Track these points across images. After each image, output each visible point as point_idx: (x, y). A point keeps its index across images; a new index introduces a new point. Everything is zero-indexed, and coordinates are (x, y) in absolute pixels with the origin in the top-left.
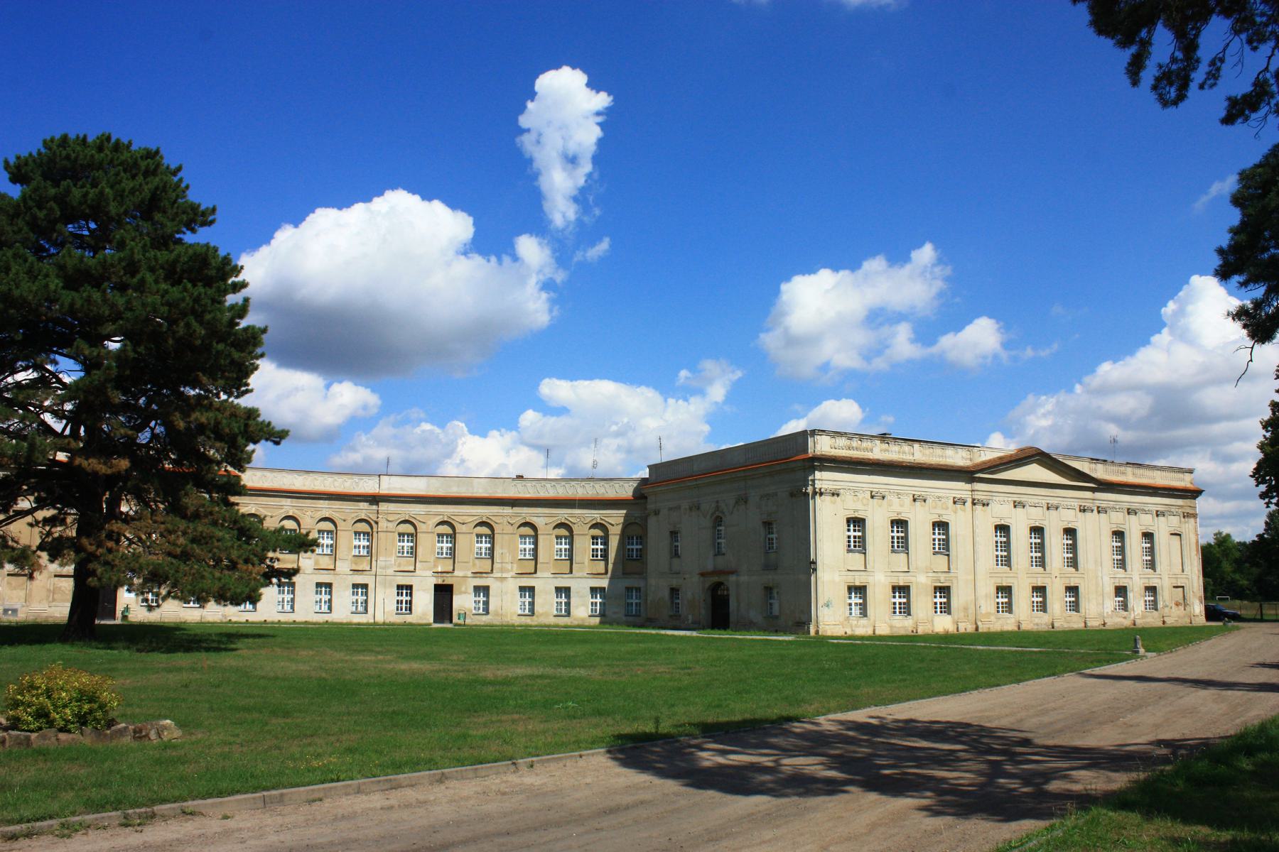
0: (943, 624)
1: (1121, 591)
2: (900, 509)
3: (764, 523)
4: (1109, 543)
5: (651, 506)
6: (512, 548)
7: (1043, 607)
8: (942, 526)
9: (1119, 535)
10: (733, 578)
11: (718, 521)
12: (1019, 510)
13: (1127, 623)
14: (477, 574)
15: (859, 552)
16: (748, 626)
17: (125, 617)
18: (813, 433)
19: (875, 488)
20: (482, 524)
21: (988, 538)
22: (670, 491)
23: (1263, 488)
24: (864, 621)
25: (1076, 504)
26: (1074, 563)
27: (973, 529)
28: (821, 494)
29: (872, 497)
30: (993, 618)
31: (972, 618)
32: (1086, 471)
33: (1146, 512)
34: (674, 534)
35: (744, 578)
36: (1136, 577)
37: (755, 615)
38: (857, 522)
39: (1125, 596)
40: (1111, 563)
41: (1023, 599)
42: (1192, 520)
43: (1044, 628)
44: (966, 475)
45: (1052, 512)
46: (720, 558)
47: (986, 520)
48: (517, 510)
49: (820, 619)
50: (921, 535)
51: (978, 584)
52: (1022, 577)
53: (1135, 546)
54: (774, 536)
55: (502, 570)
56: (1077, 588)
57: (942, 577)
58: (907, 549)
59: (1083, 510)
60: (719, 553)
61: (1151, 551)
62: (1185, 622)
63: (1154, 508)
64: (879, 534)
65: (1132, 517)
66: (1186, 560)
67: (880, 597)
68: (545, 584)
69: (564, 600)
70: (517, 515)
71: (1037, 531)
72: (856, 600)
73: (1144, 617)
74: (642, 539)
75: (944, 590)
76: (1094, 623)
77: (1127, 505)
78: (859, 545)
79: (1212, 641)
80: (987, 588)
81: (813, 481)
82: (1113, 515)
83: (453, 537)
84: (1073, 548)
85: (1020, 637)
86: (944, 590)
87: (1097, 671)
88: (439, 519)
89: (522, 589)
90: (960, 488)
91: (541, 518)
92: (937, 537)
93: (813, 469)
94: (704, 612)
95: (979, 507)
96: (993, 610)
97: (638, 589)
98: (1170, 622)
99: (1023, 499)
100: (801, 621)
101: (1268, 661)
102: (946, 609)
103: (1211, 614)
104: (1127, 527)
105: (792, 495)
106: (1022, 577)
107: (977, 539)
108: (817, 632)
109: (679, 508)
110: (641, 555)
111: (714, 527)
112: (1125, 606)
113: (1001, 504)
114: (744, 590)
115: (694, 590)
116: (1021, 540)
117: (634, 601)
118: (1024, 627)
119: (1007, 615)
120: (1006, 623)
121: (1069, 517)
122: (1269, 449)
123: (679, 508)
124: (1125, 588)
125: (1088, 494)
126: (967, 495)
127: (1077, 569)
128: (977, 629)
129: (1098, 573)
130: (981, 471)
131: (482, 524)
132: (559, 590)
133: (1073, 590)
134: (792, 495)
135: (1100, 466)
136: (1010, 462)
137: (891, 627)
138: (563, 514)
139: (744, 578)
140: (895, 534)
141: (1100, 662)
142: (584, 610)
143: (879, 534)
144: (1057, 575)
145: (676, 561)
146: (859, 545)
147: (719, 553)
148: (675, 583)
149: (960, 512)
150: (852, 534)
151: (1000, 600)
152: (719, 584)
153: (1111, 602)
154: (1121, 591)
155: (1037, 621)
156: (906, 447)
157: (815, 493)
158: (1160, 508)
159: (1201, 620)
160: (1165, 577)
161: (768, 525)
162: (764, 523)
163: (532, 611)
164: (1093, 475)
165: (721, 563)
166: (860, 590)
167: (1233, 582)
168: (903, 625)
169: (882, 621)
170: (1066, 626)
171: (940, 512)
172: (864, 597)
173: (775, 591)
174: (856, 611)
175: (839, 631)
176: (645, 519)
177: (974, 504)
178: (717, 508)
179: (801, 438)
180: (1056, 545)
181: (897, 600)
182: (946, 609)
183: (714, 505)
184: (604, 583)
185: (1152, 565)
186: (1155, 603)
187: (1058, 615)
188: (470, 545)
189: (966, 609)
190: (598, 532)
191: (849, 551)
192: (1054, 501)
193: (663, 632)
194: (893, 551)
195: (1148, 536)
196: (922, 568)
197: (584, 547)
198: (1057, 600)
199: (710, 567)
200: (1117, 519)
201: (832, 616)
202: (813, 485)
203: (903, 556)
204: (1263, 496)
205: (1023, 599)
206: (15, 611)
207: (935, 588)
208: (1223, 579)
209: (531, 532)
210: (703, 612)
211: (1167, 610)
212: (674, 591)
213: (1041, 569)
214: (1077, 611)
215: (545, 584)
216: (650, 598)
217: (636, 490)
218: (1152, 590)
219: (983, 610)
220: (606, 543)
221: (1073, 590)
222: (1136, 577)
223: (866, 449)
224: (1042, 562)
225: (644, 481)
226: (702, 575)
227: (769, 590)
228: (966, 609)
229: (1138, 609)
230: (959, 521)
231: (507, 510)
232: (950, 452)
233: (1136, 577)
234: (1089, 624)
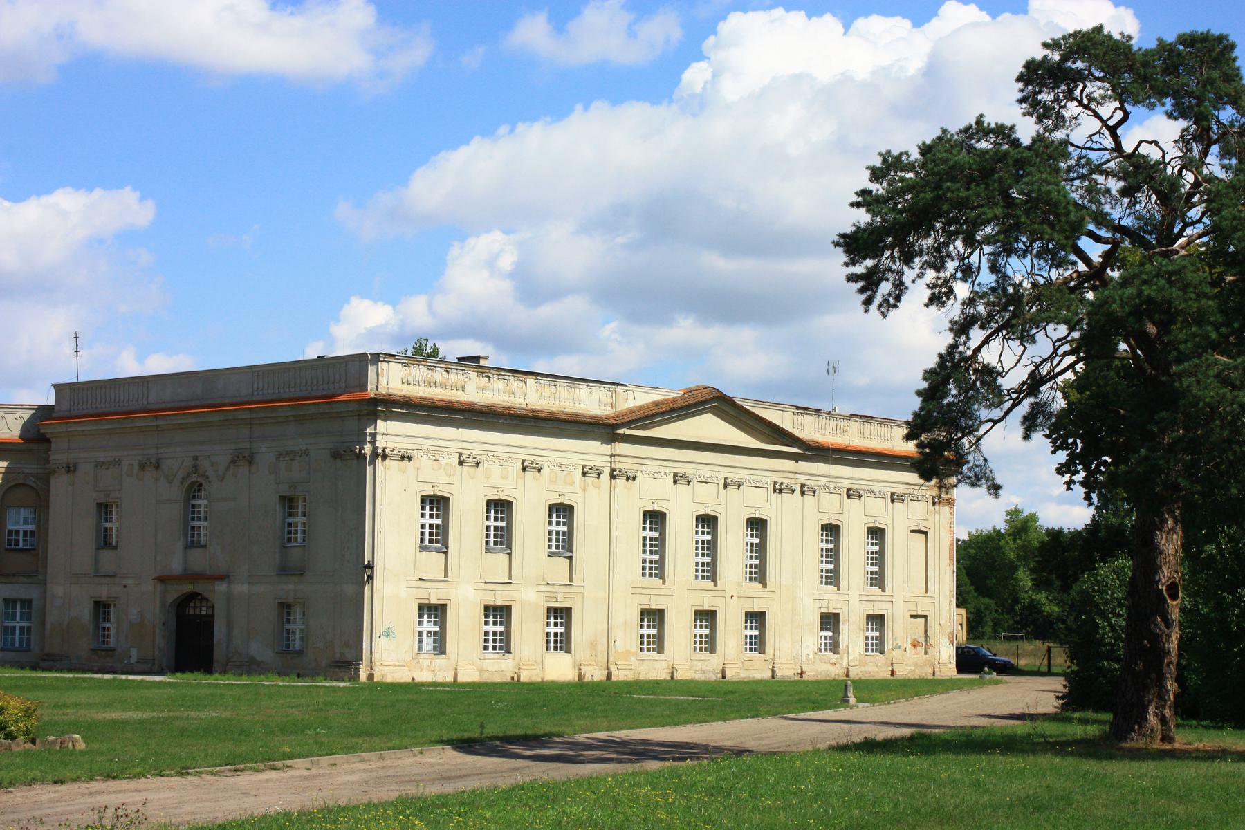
0: (559, 668)
1: (830, 621)
2: (499, 483)
3: (283, 498)
4: (815, 543)
5: (58, 456)
8: (562, 511)
9: (832, 530)
10: (221, 587)
11: (194, 490)
12: (682, 487)
15: (438, 550)
16: (251, 666)
18: (377, 358)
21: (632, 532)
23: (1062, 456)
24: (440, 661)
25: (769, 479)
26: (759, 574)
27: (609, 519)
28: (385, 457)
29: (461, 463)
30: (633, 660)
31: (602, 659)
32: (788, 426)
34: (104, 509)
35: (241, 588)
36: (854, 599)
37: (259, 649)
39: (836, 630)
40: (817, 575)
41: (680, 630)
42: (946, 509)
43: (713, 677)
44: (604, 429)
45: (732, 492)
46: (196, 554)
49: (376, 656)
50: (531, 525)
51: (613, 604)
53: (855, 547)
54: (299, 520)
56: (763, 614)
57: (561, 593)
58: (509, 546)
59: (779, 490)
60: (193, 543)
62: (926, 672)
63: (888, 489)
64: (468, 522)
65: (854, 502)
66: (931, 573)
67: (466, 624)
71: (707, 522)
72: (429, 627)
73: (862, 663)
75: (561, 614)
76: (786, 672)
77: (846, 484)
78: (437, 538)
79: (950, 695)
81: (374, 435)
82: (824, 497)
86: (561, 614)
87: (802, 715)
90: (593, 451)
92: (554, 528)
93: (373, 417)
94: (161, 642)
96: (636, 646)
97: (27, 603)
98: (902, 672)
100: (345, 659)
101: (998, 713)
102: (563, 643)
103: (968, 661)
104: (844, 518)
105: (336, 455)
106: (681, 594)
107: (616, 533)
108: (371, 677)
109: (118, 463)
111: (187, 500)
112: (834, 646)
113: (654, 478)
114: (242, 607)
115: (143, 608)
116: (682, 537)
117: (18, 624)
118: (679, 675)
119: (655, 655)
120: (653, 668)
121: (759, 502)
123: (118, 463)
124: (836, 616)
125: (788, 464)
126: (604, 464)
127: (764, 585)
128: (609, 676)
129: (796, 592)
130: (628, 424)
133: (756, 618)
134: (336, 455)
135: (809, 419)
136: (673, 410)
137: (481, 671)
139: (241, 588)
140: (492, 523)
141: (805, 710)
143: (468, 522)
145: (106, 555)
146: (437, 538)
148: (104, 593)
149: (591, 489)
150: (427, 521)
151: (646, 631)
152: (192, 596)
153: (814, 637)
154: (830, 621)
155: (699, 666)
156: (515, 383)
157: (375, 455)
158: (899, 489)
159: (949, 669)
160: (899, 600)
161: (288, 502)
162: (283, 498)
164: (798, 433)
165: (198, 560)
168: (497, 668)
169: (469, 661)
170: (744, 675)
171: (562, 488)
173: (297, 613)
174: (428, 643)
175: (402, 676)
176: (46, 479)
177: (613, 477)
178: (195, 468)
181: (491, 628)
183: (188, 463)
185: (879, 580)
187: (734, 659)
189: (593, 645)
191: (422, 549)
193: (131, 677)
194: (488, 550)
195: (876, 534)
196: (531, 579)
198: (732, 631)
199: (176, 565)
200: (830, 506)
201: (393, 651)
202: (373, 442)
203: (503, 558)
205: (680, 630)
207: (549, 609)
208: (1016, 600)
210: (160, 642)
211: (898, 652)
212: (101, 608)
213: (709, 583)
214: (762, 652)
216: (50, 620)
219: (620, 646)
223: (455, 387)
225: (43, 412)
226: (162, 580)
227: (285, 608)
228: (593, 645)
230: (591, 504)
232: (581, 391)
233: (854, 599)
234: (778, 673)
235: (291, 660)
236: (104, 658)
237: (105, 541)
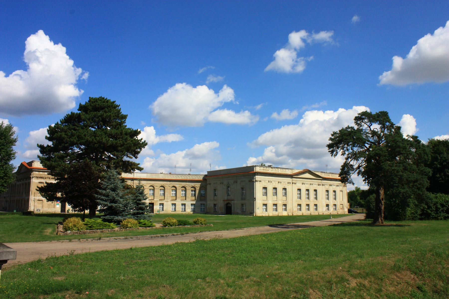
0: (285, 214)
1: (327, 205)
6: (170, 193)
7: (309, 209)
9: (327, 191)
10: (233, 202)
11: (228, 187)
12: (303, 185)
13: (329, 213)
14: (160, 200)
16: (237, 214)
17: (68, 212)
18: (255, 166)
19: (270, 180)
20: (162, 186)
21: (296, 192)
22: (211, 179)
23: (364, 178)
24: (266, 213)
25: (317, 183)
26: (316, 198)
27: (292, 190)
33: (334, 185)
34: (215, 190)
35: (236, 202)
38: (265, 188)
41: (304, 207)
44: (291, 176)
45: (311, 186)
46: (229, 197)
47: (295, 187)
48: (171, 183)
50: (280, 191)
52: (304, 202)
53: (331, 194)
55: (167, 199)
57: (285, 202)
60: (228, 195)
61: (335, 195)
62: (343, 213)
63: (336, 184)
64: (270, 191)
67: (270, 207)
68: (179, 203)
69: (184, 207)
70: (171, 184)
72: (264, 207)
74: (206, 190)
75: (285, 205)
76: (321, 214)
80: (295, 205)
82: (326, 186)
83: (154, 190)
84: (316, 195)
85: (303, 216)
86: (285, 205)
88: (150, 185)
89: (172, 204)
90: (289, 180)
91: (178, 185)
93: (255, 175)
94: (224, 210)
95: (294, 184)
96: (297, 210)
97: (204, 204)
98: (339, 213)
99: (304, 182)
100: (252, 212)
102: (286, 210)
103: (350, 211)
105: (249, 181)
106: (304, 202)
110: (205, 195)
112: (328, 209)
113: (299, 184)
114: (236, 204)
115: (221, 205)
116: (304, 192)
120: (300, 213)
122: (365, 169)
125: (320, 181)
126: (291, 181)
129: (322, 201)
130: (295, 175)
131: (162, 186)
132: (182, 204)
134: (249, 181)
135: (323, 174)
138: (184, 184)
139: (236, 202)
142: (189, 210)
143: (270, 191)
144: (312, 202)
146: (266, 194)
147: (228, 195)
148: (215, 203)
153: (325, 208)
154: (327, 205)
156: (277, 170)
158: (338, 184)
159: (347, 213)
163: (185, 210)
166: (265, 205)
167: (360, 202)
168: (275, 214)
169: (271, 213)
172: (266, 207)
173: (244, 206)
174: (264, 210)
175: (261, 215)
176: (206, 185)
178: (228, 184)
179: (252, 168)
180: (312, 193)
182: (286, 210)
184: (194, 202)
185: (335, 199)
186: (336, 209)
187: (312, 212)
188: (158, 192)
189: (290, 210)
190: (193, 189)
192: (312, 183)
195: (335, 191)
196: (280, 200)
197: (189, 193)
198: (312, 208)
199: (226, 198)
200: (327, 187)
201: (259, 211)
204: (364, 181)
205: (304, 207)
206: (40, 210)
209: (184, 189)
212: (215, 205)
215: (179, 203)
216: (207, 207)
217: (203, 178)
218: (335, 205)
219: (294, 210)
220: (195, 191)
221: (316, 205)
222: (331, 202)
224: (308, 198)
225: (206, 176)
226: (224, 201)
227: (242, 205)
228: (290, 210)
229: (332, 210)
231: (169, 183)
232: (287, 170)
233: (331, 202)
235: (244, 213)
236: (215, 212)
237: (215, 195)
